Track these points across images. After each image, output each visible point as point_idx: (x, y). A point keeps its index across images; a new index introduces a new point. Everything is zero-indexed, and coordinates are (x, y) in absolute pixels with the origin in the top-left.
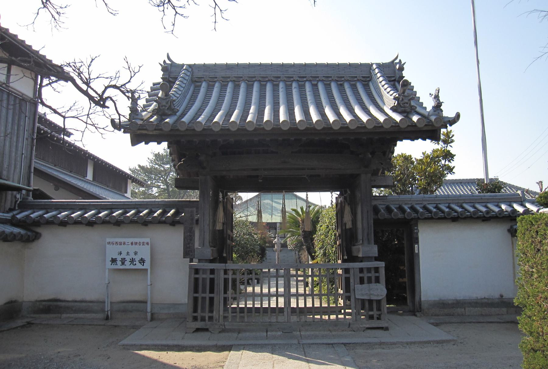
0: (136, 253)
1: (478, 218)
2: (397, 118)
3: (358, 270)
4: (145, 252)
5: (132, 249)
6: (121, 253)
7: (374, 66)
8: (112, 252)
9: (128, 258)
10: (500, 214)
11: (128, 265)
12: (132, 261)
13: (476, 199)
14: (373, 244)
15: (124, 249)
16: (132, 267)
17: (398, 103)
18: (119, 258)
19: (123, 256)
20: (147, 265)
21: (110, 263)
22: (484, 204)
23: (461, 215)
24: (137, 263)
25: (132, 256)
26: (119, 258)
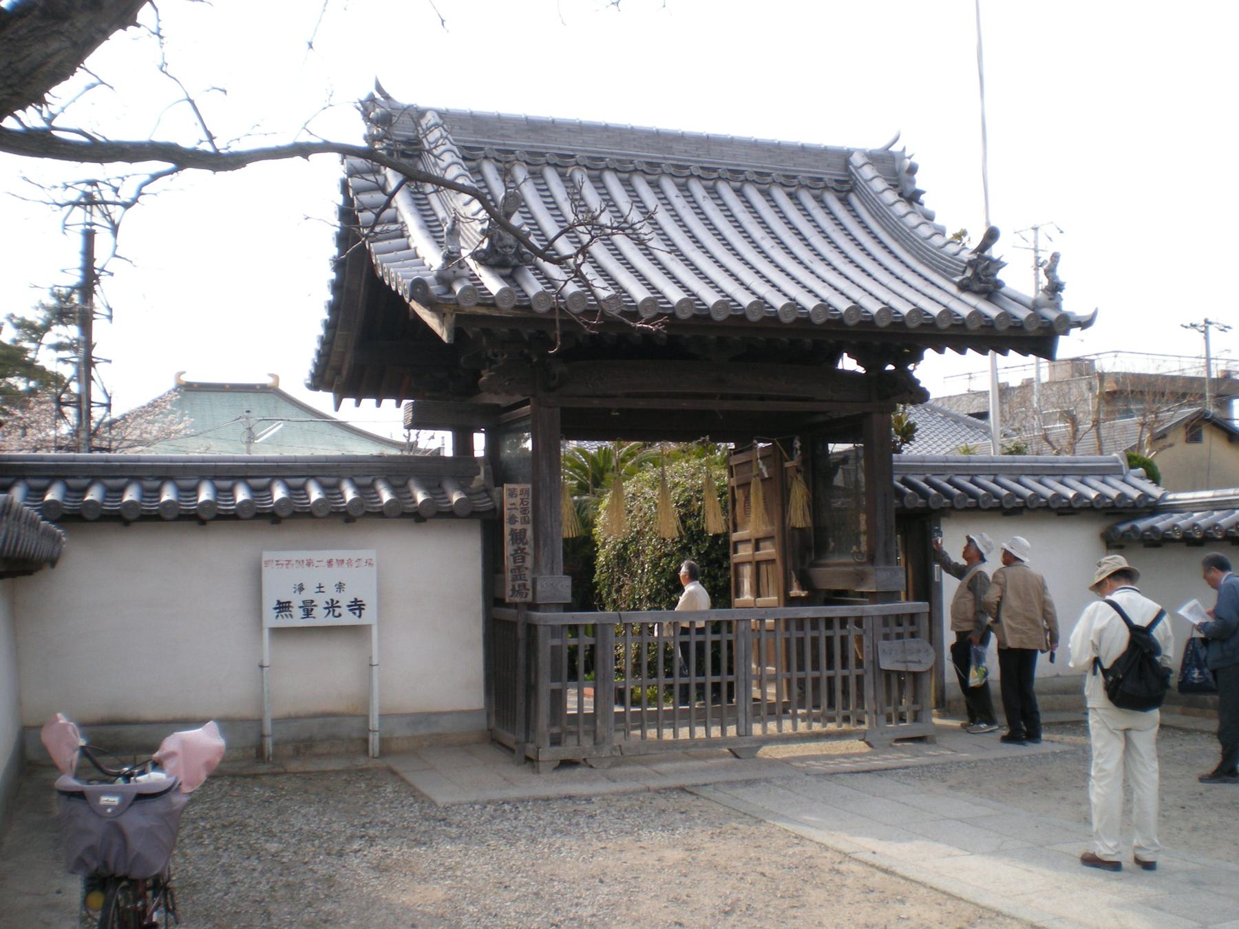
0: (340, 587)
1: (1082, 509)
2: (493, 284)
3: (881, 620)
4: (361, 584)
5: (330, 577)
6: (301, 588)
7: (430, 119)
8: (278, 585)
9: (321, 601)
10: (1098, 502)
11: (320, 618)
12: (332, 606)
13: (1045, 468)
14: (561, 575)
15: (311, 578)
16: (331, 621)
17: (491, 244)
18: (297, 601)
19: (308, 595)
20: (369, 616)
21: (275, 613)
22: (1059, 478)
23: (1032, 502)
24: (344, 610)
25: (331, 593)
26: (297, 601)
